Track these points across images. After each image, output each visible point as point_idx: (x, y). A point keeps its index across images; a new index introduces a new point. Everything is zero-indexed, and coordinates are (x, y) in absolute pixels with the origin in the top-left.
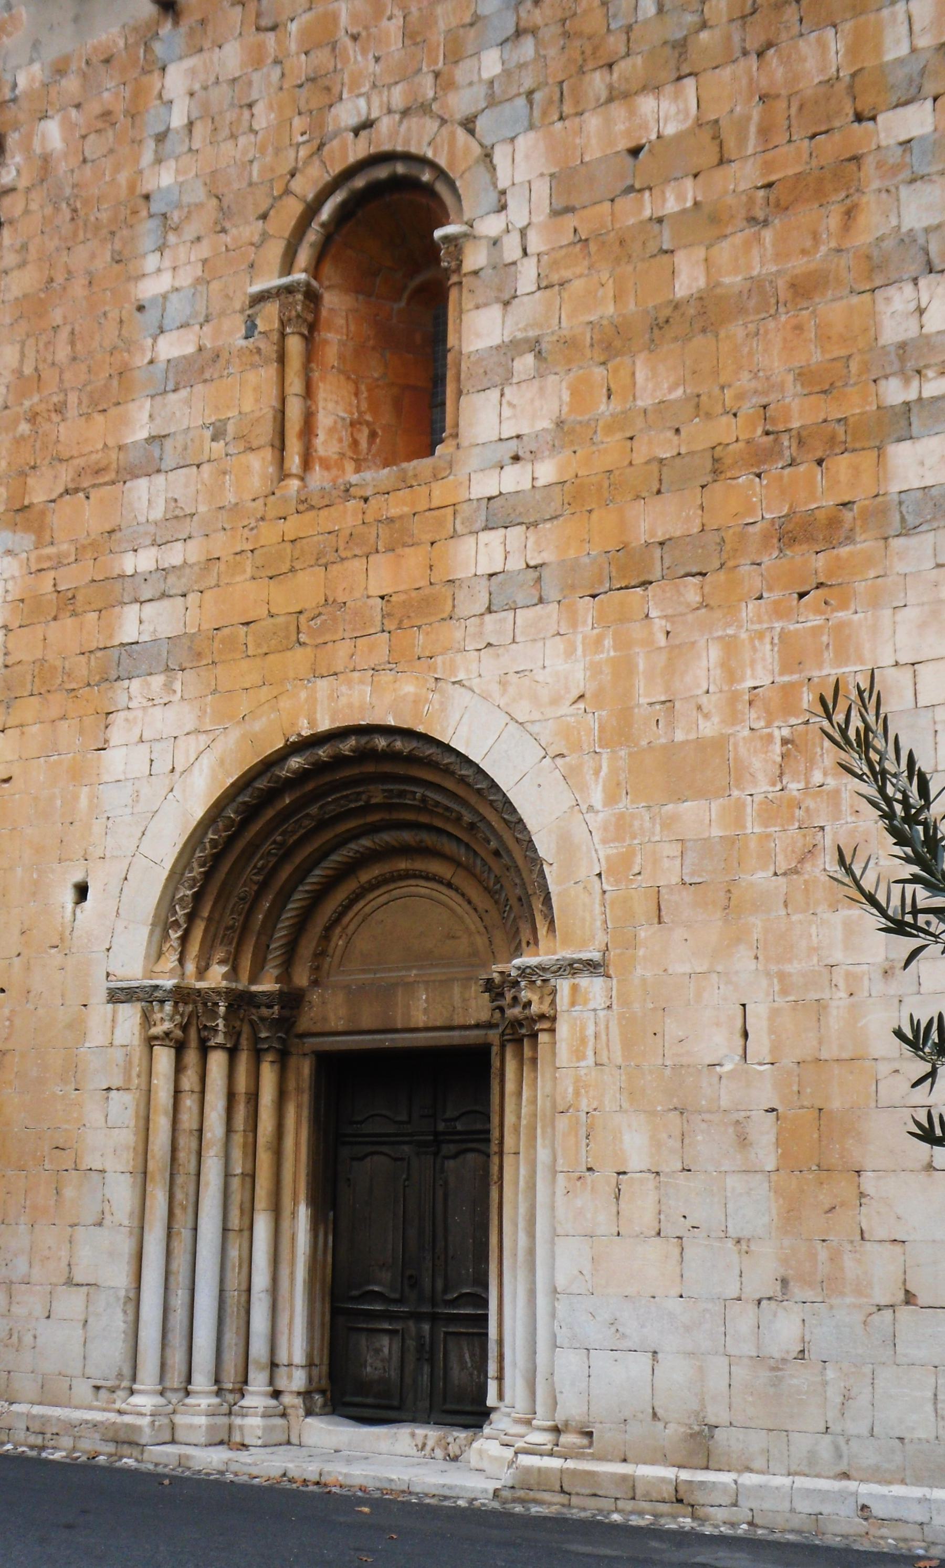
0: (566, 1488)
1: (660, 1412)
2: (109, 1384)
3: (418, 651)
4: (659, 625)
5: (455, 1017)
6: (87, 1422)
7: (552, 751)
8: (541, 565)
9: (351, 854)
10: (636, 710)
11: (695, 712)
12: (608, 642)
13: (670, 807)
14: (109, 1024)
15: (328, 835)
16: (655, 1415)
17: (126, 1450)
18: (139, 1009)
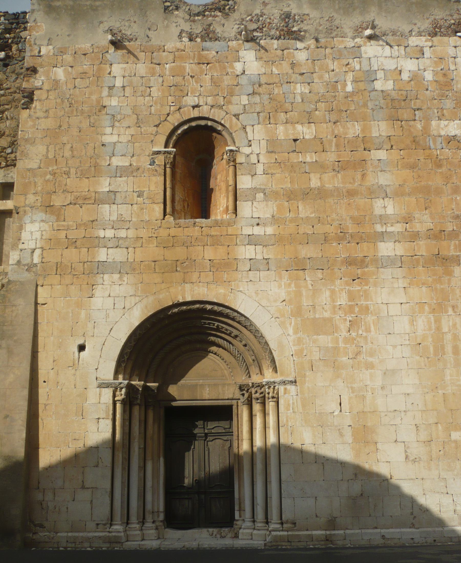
0: (290, 540)
1: (318, 515)
2: (104, 522)
3: (225, 279)
4: (309, 282)
6: (96, 537)
7: (275, 316)
12: (293, 285)
13: (315, 336)
14: (98, 395)
18: (112, 390)
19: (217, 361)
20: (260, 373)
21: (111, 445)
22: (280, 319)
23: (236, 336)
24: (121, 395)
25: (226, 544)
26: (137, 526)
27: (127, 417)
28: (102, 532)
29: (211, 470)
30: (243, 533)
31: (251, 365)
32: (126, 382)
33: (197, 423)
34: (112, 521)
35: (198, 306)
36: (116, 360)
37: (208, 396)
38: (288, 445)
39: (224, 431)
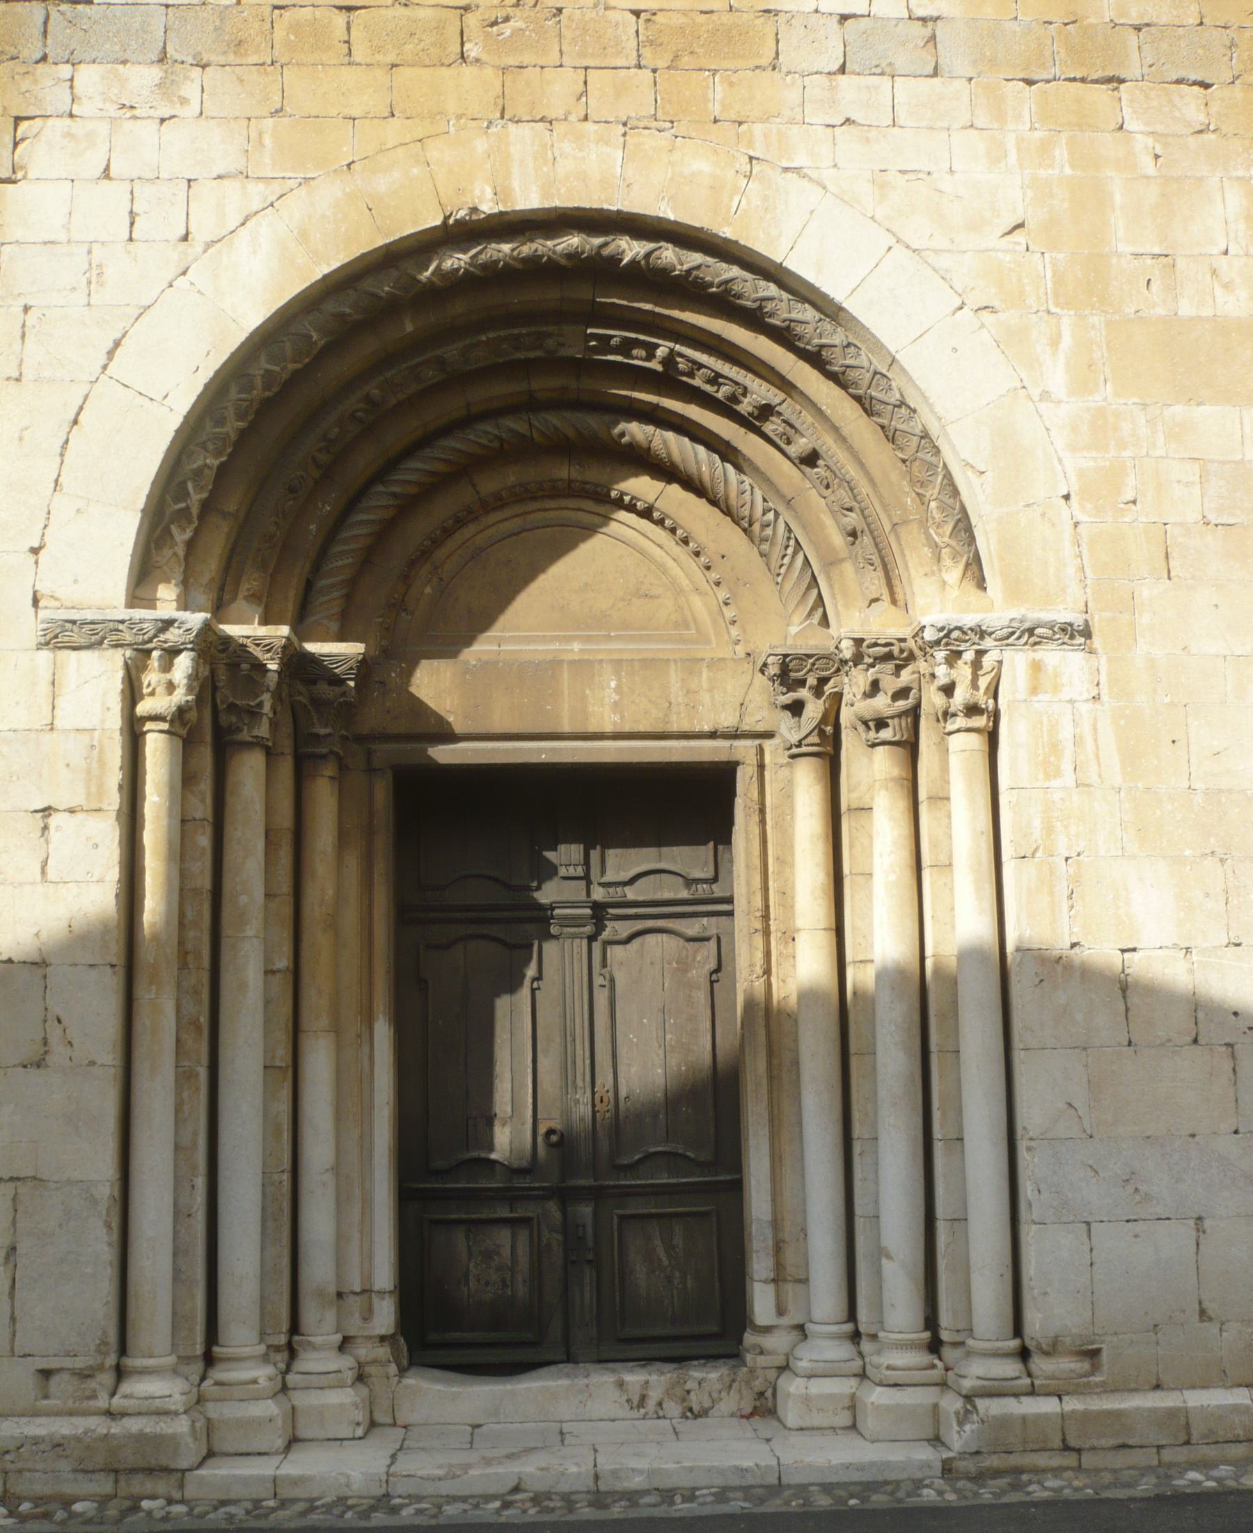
0: (1072, 1442)
1: (1212, 1308)
2: (80, 1363)
3: (717, 110)
4: (1142, 143)
5: (674, 717)
6: (36, 1441)
7: (974, 300)
8: (938, 18)
9: (484, 441)
10: (1114, 261)
11: (1208, 277)
12: (1061, 153)
13: (1178, 409)
14: (45, 688)
15: (453, 405)
16: (1202, 1312)
17: (138, 1485)
18: (120, 663)
19: (656, 552)
20: (886, 596)
21: (115, 951)
22: (1001, 316)
23: (766, 411)
24: (171, 687)
25: (742, 1471)
26: (264, 1374)
27: (202, 808)
28: (71, 1413)
29: (621, 1080)
30: (806, 1399)
31: (831, 563)
32: (196, 619)
33: (550, 855)
34: (123, 1350)
35: (574, 241)
36: (141, 502)
37: (617, 718)
38: (1056, 953)
39: (684, 894)
